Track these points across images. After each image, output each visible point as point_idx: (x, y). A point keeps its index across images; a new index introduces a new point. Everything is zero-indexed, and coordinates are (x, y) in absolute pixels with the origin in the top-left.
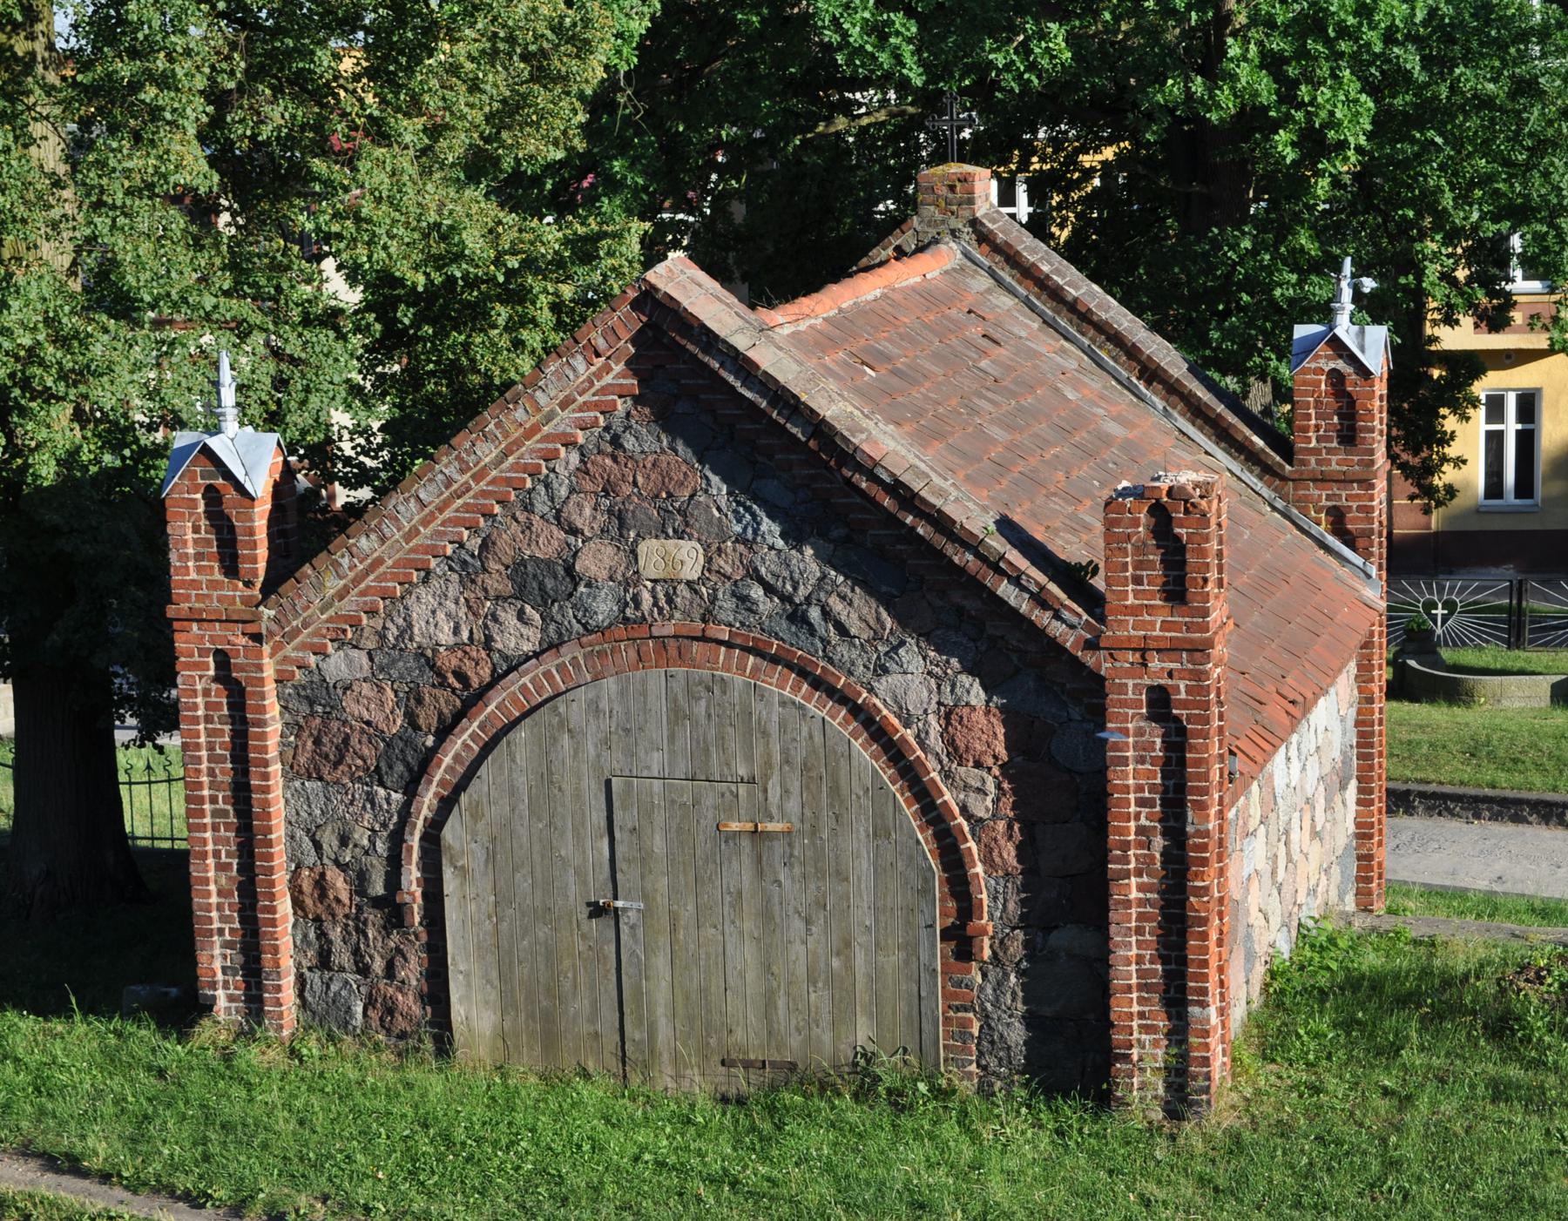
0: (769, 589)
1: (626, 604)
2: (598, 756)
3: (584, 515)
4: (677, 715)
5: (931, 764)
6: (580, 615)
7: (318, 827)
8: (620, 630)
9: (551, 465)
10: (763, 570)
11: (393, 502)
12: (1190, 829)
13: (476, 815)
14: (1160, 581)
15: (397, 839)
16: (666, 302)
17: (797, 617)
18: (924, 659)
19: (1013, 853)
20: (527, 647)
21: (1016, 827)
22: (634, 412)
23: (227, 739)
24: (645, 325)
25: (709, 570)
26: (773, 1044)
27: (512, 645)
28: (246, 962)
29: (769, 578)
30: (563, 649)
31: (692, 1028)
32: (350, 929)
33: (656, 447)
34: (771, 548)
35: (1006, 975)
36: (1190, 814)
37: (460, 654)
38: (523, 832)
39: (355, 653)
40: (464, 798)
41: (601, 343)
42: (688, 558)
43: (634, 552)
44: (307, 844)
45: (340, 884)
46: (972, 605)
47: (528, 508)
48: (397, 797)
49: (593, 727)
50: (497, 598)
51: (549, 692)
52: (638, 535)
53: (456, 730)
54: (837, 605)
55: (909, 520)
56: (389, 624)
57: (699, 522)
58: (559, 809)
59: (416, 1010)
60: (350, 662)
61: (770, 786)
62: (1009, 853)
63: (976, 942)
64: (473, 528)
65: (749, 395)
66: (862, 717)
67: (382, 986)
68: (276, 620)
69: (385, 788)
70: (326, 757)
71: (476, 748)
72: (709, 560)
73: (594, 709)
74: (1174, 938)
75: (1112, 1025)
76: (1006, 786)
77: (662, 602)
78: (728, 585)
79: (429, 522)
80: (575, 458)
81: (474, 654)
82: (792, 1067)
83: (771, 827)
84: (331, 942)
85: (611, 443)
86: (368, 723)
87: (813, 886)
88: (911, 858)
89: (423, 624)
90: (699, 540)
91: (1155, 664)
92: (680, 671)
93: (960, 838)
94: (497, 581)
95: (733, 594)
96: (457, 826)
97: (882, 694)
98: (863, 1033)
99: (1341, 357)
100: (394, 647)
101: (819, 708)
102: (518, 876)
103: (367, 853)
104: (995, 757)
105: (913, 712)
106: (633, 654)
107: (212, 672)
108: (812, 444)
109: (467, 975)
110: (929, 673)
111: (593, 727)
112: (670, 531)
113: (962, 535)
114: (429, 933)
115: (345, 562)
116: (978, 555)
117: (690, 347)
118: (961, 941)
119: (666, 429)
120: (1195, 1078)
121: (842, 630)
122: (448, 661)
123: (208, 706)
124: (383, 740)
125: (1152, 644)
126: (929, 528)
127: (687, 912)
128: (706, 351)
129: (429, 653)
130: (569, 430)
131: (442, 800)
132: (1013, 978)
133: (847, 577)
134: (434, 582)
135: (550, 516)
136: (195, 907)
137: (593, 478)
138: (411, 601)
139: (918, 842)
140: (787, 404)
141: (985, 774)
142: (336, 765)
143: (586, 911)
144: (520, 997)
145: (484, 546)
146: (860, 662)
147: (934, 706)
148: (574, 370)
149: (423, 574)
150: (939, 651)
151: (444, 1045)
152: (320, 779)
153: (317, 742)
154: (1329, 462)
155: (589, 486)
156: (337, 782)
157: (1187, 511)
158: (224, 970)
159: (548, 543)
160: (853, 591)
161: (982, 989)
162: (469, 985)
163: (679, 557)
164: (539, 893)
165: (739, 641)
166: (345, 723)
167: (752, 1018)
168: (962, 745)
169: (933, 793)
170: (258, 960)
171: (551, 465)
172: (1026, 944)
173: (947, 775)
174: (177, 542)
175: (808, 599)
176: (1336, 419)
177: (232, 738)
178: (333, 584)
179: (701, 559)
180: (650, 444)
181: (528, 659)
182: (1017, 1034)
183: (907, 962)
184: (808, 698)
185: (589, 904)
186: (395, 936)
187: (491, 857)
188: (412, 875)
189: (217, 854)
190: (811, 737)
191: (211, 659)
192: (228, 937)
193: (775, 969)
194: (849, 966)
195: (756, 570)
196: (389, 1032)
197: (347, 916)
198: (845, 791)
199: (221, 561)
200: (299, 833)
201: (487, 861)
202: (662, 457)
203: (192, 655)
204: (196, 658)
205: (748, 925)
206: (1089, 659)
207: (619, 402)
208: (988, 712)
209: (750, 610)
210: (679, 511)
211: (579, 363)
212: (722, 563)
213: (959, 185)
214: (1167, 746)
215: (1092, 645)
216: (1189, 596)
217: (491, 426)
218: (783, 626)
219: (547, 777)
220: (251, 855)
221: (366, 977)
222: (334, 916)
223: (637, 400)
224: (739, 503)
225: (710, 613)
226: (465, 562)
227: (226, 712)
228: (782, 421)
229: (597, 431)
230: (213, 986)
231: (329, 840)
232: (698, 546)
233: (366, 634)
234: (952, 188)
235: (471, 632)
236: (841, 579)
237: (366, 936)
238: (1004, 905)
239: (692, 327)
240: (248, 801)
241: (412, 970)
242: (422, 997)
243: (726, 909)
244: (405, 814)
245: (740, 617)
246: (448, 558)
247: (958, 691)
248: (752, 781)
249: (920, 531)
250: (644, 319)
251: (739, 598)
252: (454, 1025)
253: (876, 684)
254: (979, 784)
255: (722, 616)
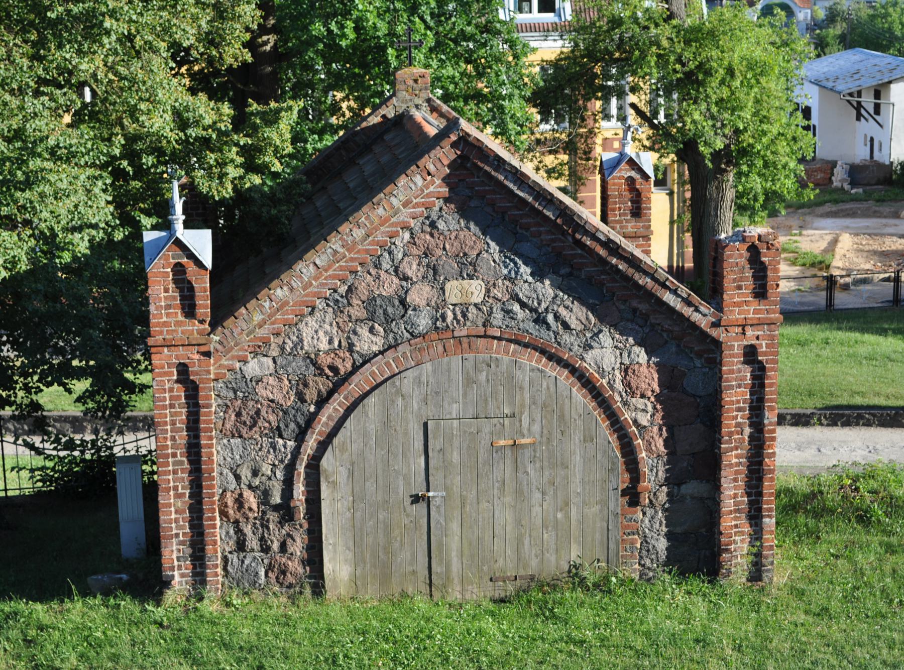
0: (523, 305)
1: (437, 319)
2: (419, 409)
3: (412, 269)
4: (469, 381)
5: (617, 398)
6: (409, 327)
7: (238, 466)
8: (434, 336)
9: (393, 240)
10: (521, 295)
11: (300, 266)
12: (766, 422)
13: (343, 449)
14: (752, 287)
15: (290, 469)
16: (475, 143)
17: (540, 320)
18: (613, 339)
19: (662, 444)
20: (375, 348)
21: (664, 429)
22: (444, 207)
23: (184, 417)
24: (459, 157)
25: (488, 297)
26: (521, 565)
27: (366, 348)
28: (193, 552)
29: (525, 300)
30: (400, 348)
31: (473, 562)
32: (258, 525)
33: (457, 227)
34: (526, 281)
35: (656, 512)
36: (767, 413)
37: (333, 355)
38: (372, 458)
39: (265, 359)
40: (336, 441)
41: (431, 168)
42: (475, 290)
43: (443, 289)
44: (231, 477)
45: (251, 499)
46: (643, 307)
47: (378, 266)
48: (291, 444)
49: (417, 392)
50: (357, 320)
51: (388, 374)
52: (445, 278)
53: (330, 401)
54: (563, 312)
55: (614, 261)
56: (287, 341)
57: (482, 269)
58: (395, 442)
59: (300, 570)
60: (261, 365)
61: (523, 418)
62: (659, 444)
63: (642, 495)
64: (343, 281)
65: (521, 194)
66: (577, 374)
67: (278, 558)
68: (220, 343)
69: (283, 438)
70: (245, 423)
71: (342, 411)
72: (488, 291)
73: (418, 381)
74: (754, 482)
75: (721, 533)
76: (659, 407)
77: (459, 317)
78: (499, 304)
79: (318, 278)
80: (407, 236)
81: (342, 355)
82: (532, 578)
83: (523, 441)
84: (245, 535)
85: (430, 226)
86: (272, 401)
87: (547, 473)
88: (605, 452)
89: (310, 339)
90: (483, 279)
91: (750, 332)
92: (471, 356)
93: (634, 438)
94: (357, 311)
95: (503, 309)
96: (331, 457)
97: (588, 360)
98: (574, 554)
99: (633, 169)
100: (290, 354)
101: (552, 370)
102: (368, 484)
103: (270, 479)
104: (653, 391)
105: (606, 369)
106: (440, 348)
107: (175, 378)
108: (559, 221)
109: (334, 545)
110: (616, 347)
111: (417, 392)
112: (465, 276)
113: (645, 268)
114: (309, 523)
115: (267, 304)
116: (654, 279)
117: (487, 168)
118: (632, 495)
119: (462, 216)
120: (766, 558)
121: (566, 326)
122: (325, 361)
123: (171, 398)
124: (282, 410)
125: (749, 322)
126: (626, 265)
127: (472, 495)
128: (496, 170)
129: (313, 356)
130: (406, 219)
131: (320, 443)
132: (660, 514)
133: (569, 296)
134: (317, 314)
135: (391, 271)
136: (161, 522)
137: (418, 247)
138: (301, 326)
139: (609, 442)
140: (545, 199)
141: (647, 402)
142: (251, 428)
143: (410, 500)
144: (368, 555)
145: (350, 290)
146: (576, 343)
147: (618, 365)
148: (415, 184)
149: (310, 309)
150: (621, 334)
151: (318, 589)
152: (241, 437)
153: (239, 415)
154: (627, 227)
155: (415, 251)
156: (251, 438)
157: (768, 248)
158: (178, 559)
159: (390, 286)
160: (573, 303)
161: (642, 521)
162: (335, 551)
163: (470, 290)
164: (380, 493)
165: (506, 336)
166: (257, 402)
167: (509, 552)
168: (634, 385)
169: (619, 414)
170: (203, 550)
171: (393, 240)
172: (668, 494)
173: (625, 404)
174: (155, 299)
175: (547, 310)
176: (629, 203)
177: (187, 416)
178: (257, 318)
179: (483, 290)
180: (454, 225)
181: (376, 355)
182: (662, 544)
183: (601, 511)
184: (546, 366)
185: (411, 496)
186: (286, 527)
187: (351, 474)
188: (299, 490)
189: (176, 488)
190: (548, 388)
191: (175, 370)
192: (181, 538)
193: (523, 522)
194: (568, 517)
195: (517, 295)
196: (281, 584)
197: (255, 518)
198: (567, 417)
199: (183, 309)
200: (225, 471)
201: (348, 477)
202: (461, 233)
203: (163, 368)
204: (166, 369)
205: (508, 499)
206: (714, 333)
207: (437, 201)
208: (649, 366)
209: (512, 318)
210: (470, 264)
211: (418, 180)
212: (496, 292)
213: (420, 80)
214: (754, 377)
215: (716, 325)
216: (769, 294)
217: (363, 219)
218: (531, 326)
219: (387, 423)
220: (200, 487)
221: (267, 553)
222: (247, 519)
223: (447, 200)
224: (506, 257)
225: (488, 321)
226: (337, 301)
227: (183, 400)
228: (541, 208)
229: (421, 219)
230: (172, 569)
231: (245, 473)
232: (482, 283)
233: (272, 348)
234: (416, 81)
235: (340, 342)
236: (566, 297)
237: (268, 528)
238: (657, 474)
239: (488, 157)
240: (198, 454)
241: (298, 547)
242: (303, 562)
243: (495, 491)
244: (296, 453)
245: (506, 323)
246: (326, 299)
247: (632, 356)
248: (513, 416)
249: (620, 267)
250: (459, 153)
251: (505, 312)
252: (326, 576)
253: (585, 355)
254: (643, 407)
255: (495, 323)
